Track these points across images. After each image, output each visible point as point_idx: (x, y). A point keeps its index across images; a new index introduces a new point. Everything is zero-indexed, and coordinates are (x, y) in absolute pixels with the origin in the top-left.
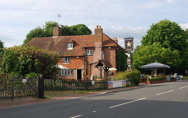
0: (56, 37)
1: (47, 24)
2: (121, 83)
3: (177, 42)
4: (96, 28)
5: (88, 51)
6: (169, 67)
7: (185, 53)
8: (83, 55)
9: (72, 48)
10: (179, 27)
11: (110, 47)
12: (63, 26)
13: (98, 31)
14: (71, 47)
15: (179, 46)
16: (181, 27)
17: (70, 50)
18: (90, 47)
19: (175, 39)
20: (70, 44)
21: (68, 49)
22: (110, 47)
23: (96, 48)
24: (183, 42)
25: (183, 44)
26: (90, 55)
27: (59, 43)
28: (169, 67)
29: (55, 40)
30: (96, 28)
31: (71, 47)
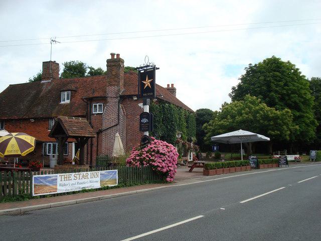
0: (47, 81)
1: (66, 67)
2: (98, 179)
3: (292, 95)
4: (110, 57)
5: (95, 106)
6: (269, 139)
7: (305, 115)
8: (85, 114)
9: (68, 102)
10: (298, 69)
11: (135, 95)
12: (93, 69)
13: (113, 64)
14: (68, 99)
15: (295, 102)
16: (299, 71)
17: (65, 104)
18: (98, 97)
19: (287, 90)
20: (66, 93)
21: (62, 102)
22: (135, 95)
23: (109, 100)
24: (302, 97)
25: (302, 100)
26: (98, 114)
27: (50, 91)
28: (269, 139)
29: (44, 86)
30: (110, 57)
31: (68, 99)
